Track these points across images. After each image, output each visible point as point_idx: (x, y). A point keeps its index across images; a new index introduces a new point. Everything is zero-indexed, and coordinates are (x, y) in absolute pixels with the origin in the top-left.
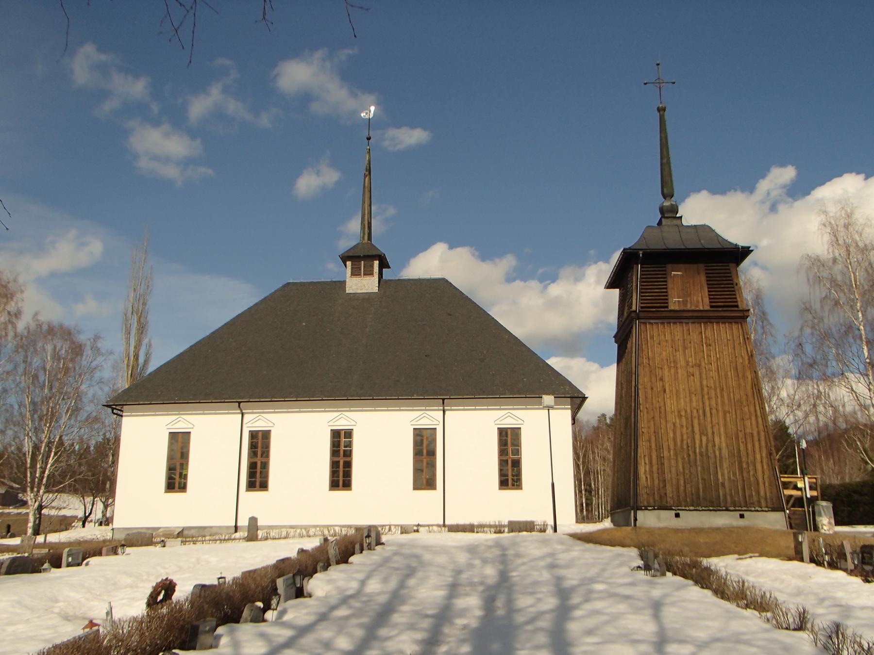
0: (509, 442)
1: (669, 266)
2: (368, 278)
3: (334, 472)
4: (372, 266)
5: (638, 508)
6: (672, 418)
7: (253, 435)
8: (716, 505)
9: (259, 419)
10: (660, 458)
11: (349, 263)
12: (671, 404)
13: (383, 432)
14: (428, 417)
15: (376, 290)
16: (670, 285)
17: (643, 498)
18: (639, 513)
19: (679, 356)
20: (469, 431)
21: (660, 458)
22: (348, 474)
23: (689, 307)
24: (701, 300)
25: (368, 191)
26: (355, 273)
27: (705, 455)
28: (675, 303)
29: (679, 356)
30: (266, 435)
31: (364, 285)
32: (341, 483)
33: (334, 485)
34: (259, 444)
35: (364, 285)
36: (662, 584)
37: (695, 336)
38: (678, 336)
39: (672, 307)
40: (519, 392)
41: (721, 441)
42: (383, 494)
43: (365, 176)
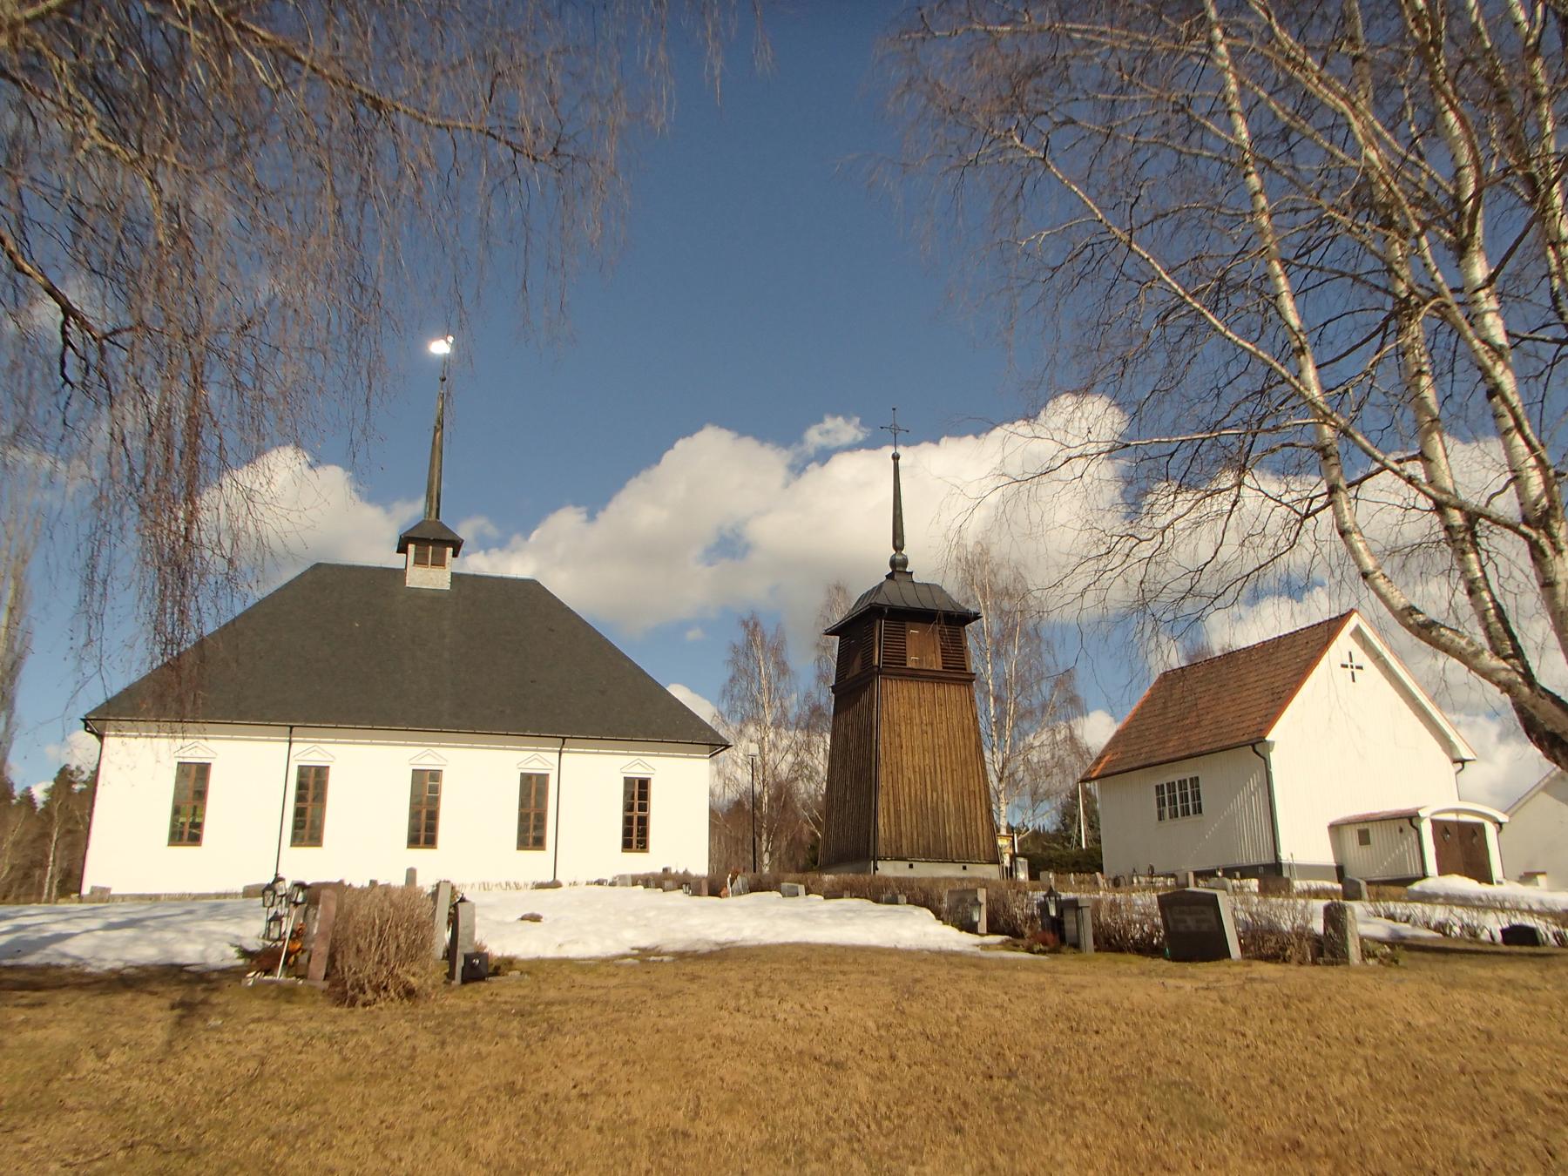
0: (638, 793)
1: (908, 624)
2: (437, 570)
3: (627, 832)
4: (444, 555)
5: (876, 858)
6: (909, 773)
7: (303, 771)
8: (944, 858)
9: (312, 750)
10: (897, 812)
11: (411, 547)
12: (907, 760)
13: (480, 776)
14: (539, 759)
15: (447, 587)
16: (908, 642)
17: (882, 849)
18: (879, 864)
19: (915, 712)
20: (589, 779)
21: (897, 812)
22: (644, 833)
23: (925, 667)
24: (935, 662)
25: (437, 449)
26: (420, 561)
27: (935, 810)
28: (912, 661)
29: (915, 712)
30: (436, 775)
31: (428, 578)
32: (422, 839)
33: (523, 844)
34: (533, 791)
35: (428, 578)
36: (1427, 925)
37: (928, 696)
38: (914, 694)
39: (909, 665)
40: (653, 735)
41: (948, 797)
42: (475, 854)
43: (436, 430)
